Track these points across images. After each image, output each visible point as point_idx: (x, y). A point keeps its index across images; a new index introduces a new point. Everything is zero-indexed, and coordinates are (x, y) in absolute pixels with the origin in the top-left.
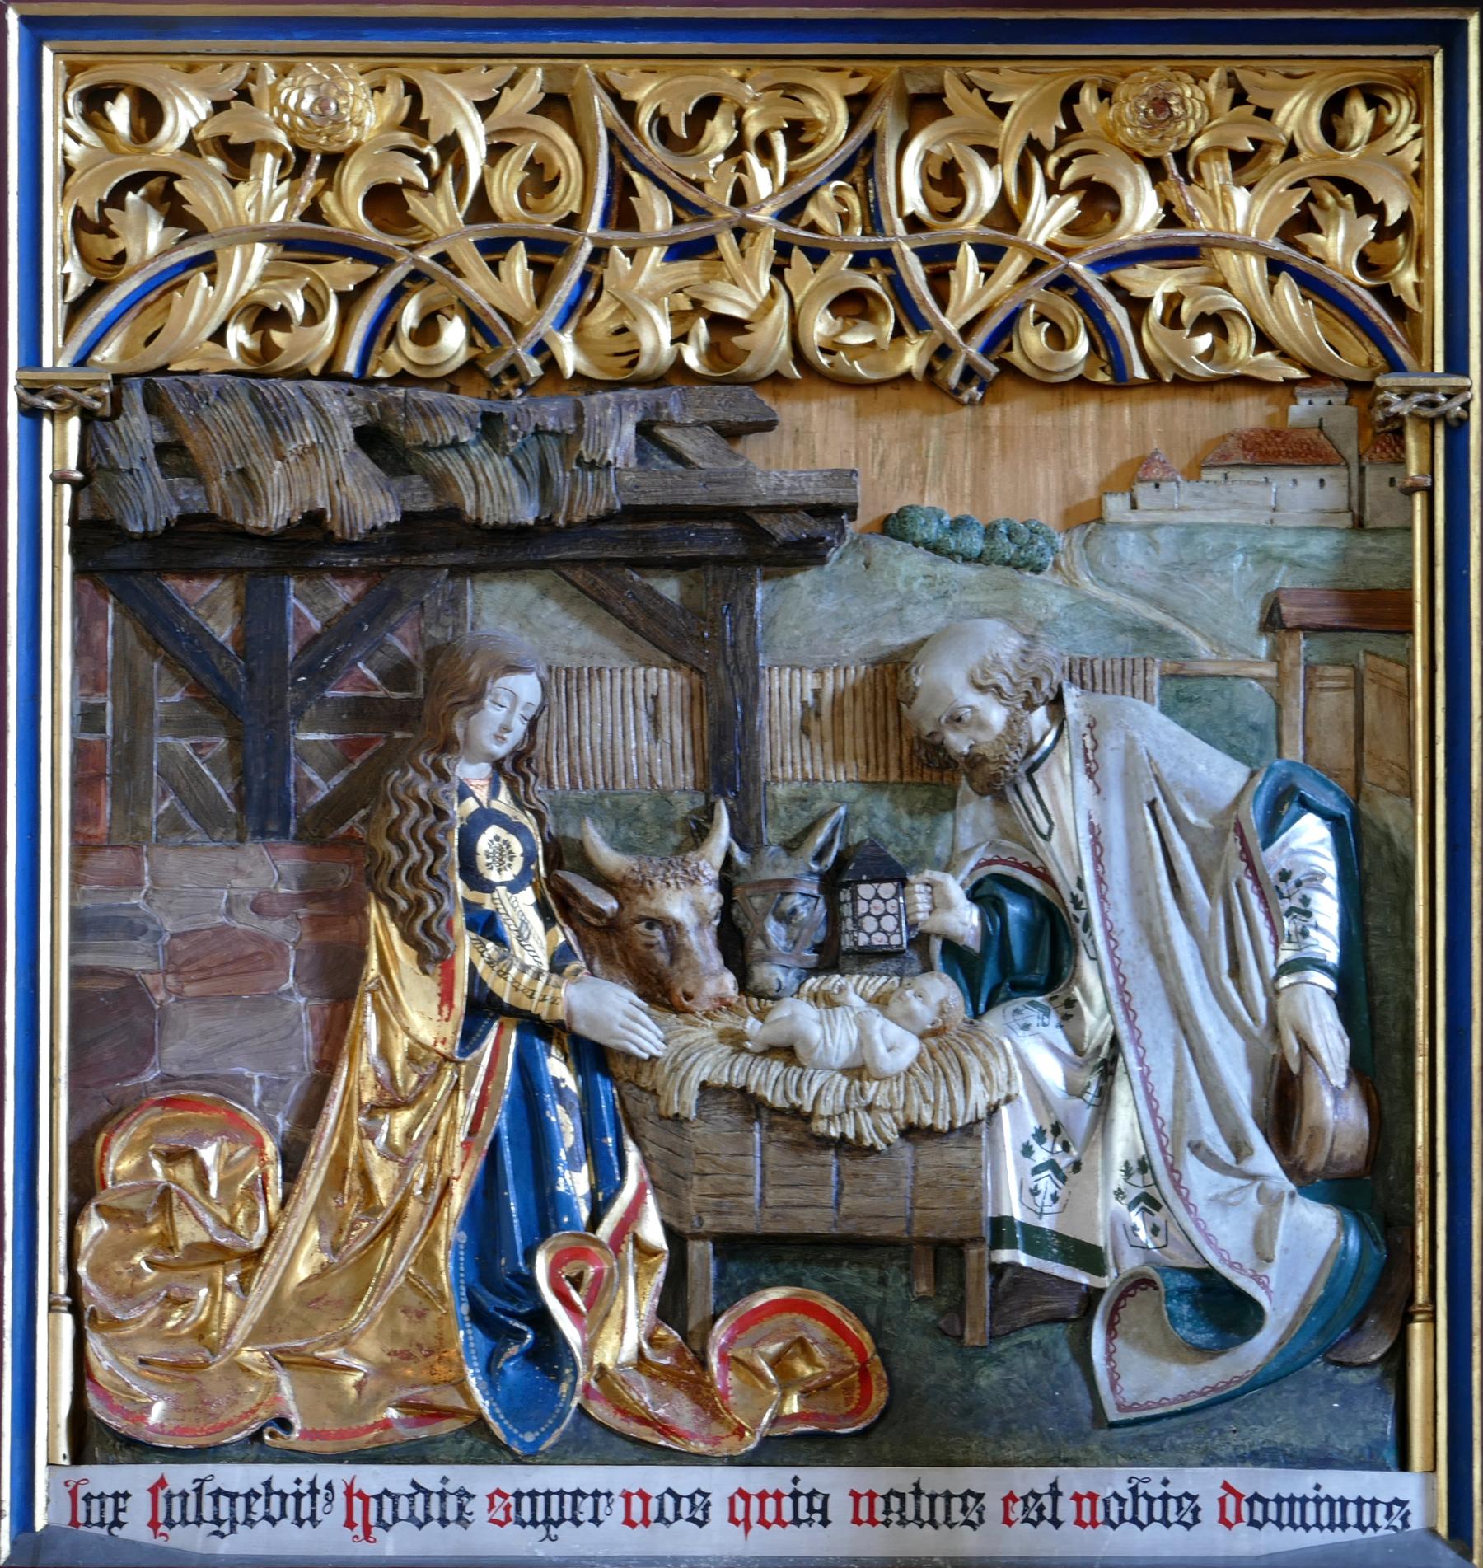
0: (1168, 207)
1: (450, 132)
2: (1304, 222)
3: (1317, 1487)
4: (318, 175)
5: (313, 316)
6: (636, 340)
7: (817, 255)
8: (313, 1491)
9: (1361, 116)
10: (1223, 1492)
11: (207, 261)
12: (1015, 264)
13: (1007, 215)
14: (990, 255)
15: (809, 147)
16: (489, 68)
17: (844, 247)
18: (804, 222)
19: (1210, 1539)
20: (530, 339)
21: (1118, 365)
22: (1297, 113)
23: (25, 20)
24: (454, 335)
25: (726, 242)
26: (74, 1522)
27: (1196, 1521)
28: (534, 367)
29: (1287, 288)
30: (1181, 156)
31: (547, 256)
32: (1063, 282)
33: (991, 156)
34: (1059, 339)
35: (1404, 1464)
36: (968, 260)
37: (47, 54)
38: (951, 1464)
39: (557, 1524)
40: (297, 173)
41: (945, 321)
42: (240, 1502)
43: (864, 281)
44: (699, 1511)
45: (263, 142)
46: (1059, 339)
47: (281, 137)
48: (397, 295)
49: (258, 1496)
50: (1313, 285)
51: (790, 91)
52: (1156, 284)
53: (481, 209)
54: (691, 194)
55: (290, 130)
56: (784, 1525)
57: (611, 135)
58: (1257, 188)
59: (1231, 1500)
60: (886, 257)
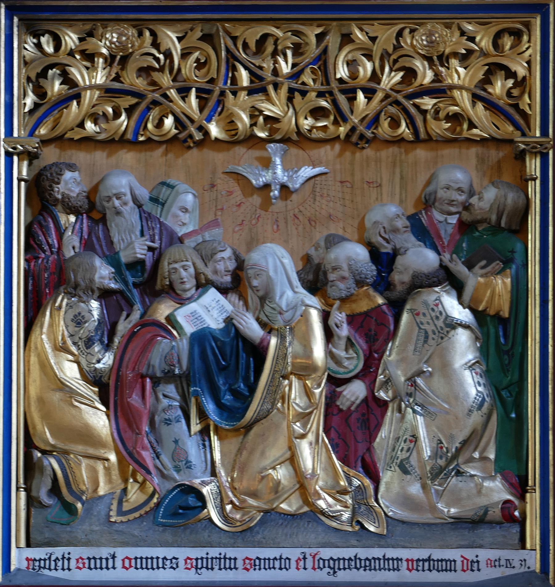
0: (436, 75)
1: (167, 48)
2: (487, 80)
3: (207, 554)
4: (118, 64)
5: (117, 115)
6: (236, 125)
7: (304, 93)
8: (63, 558)
9: (507, 42)
10: (462, 559)
11: (78, 97)
12: (380, 95)
13: (375, 77)
14: (370, 93)
15: (302, 54)
16: (83, 24)
17: (313, 90)
18: (300, 82)
19: (119, 574)
20: (196, 125)
21: (416, 132)
22: (485, 41)
23: (7, 8)
24: (169, 122)
25: (271, 88)
26: (28, 568)
27: (177, 567)
28: (198, 136)
29: (480, 106)
30: (440, 57)
31: (203, 95)
32: (397, 103)
33: (369, 57)
34: (395, 124)
35: (523, 547)
36: (361, 96)
37: (16, 20)
38: (98, 546)
39: (200, 569)
40: (111, 65)
41: (352, 117)
42: (346, 562)
43: (324, 103)
44: (174, 564)
45: (97, 53)
46: (395, 124)
47: (104, 51)
48: (148, 109)
49: (352, 560)
50: (491, 105)
51: (296, 33)
52: (428, 103)
53: (176, 76)
54: (259, 72)
55: (109, 49)
56: (148, 569)
57: (228, 50)
58: (468, 69)
59: (465, 561)
60: (331, 93)
